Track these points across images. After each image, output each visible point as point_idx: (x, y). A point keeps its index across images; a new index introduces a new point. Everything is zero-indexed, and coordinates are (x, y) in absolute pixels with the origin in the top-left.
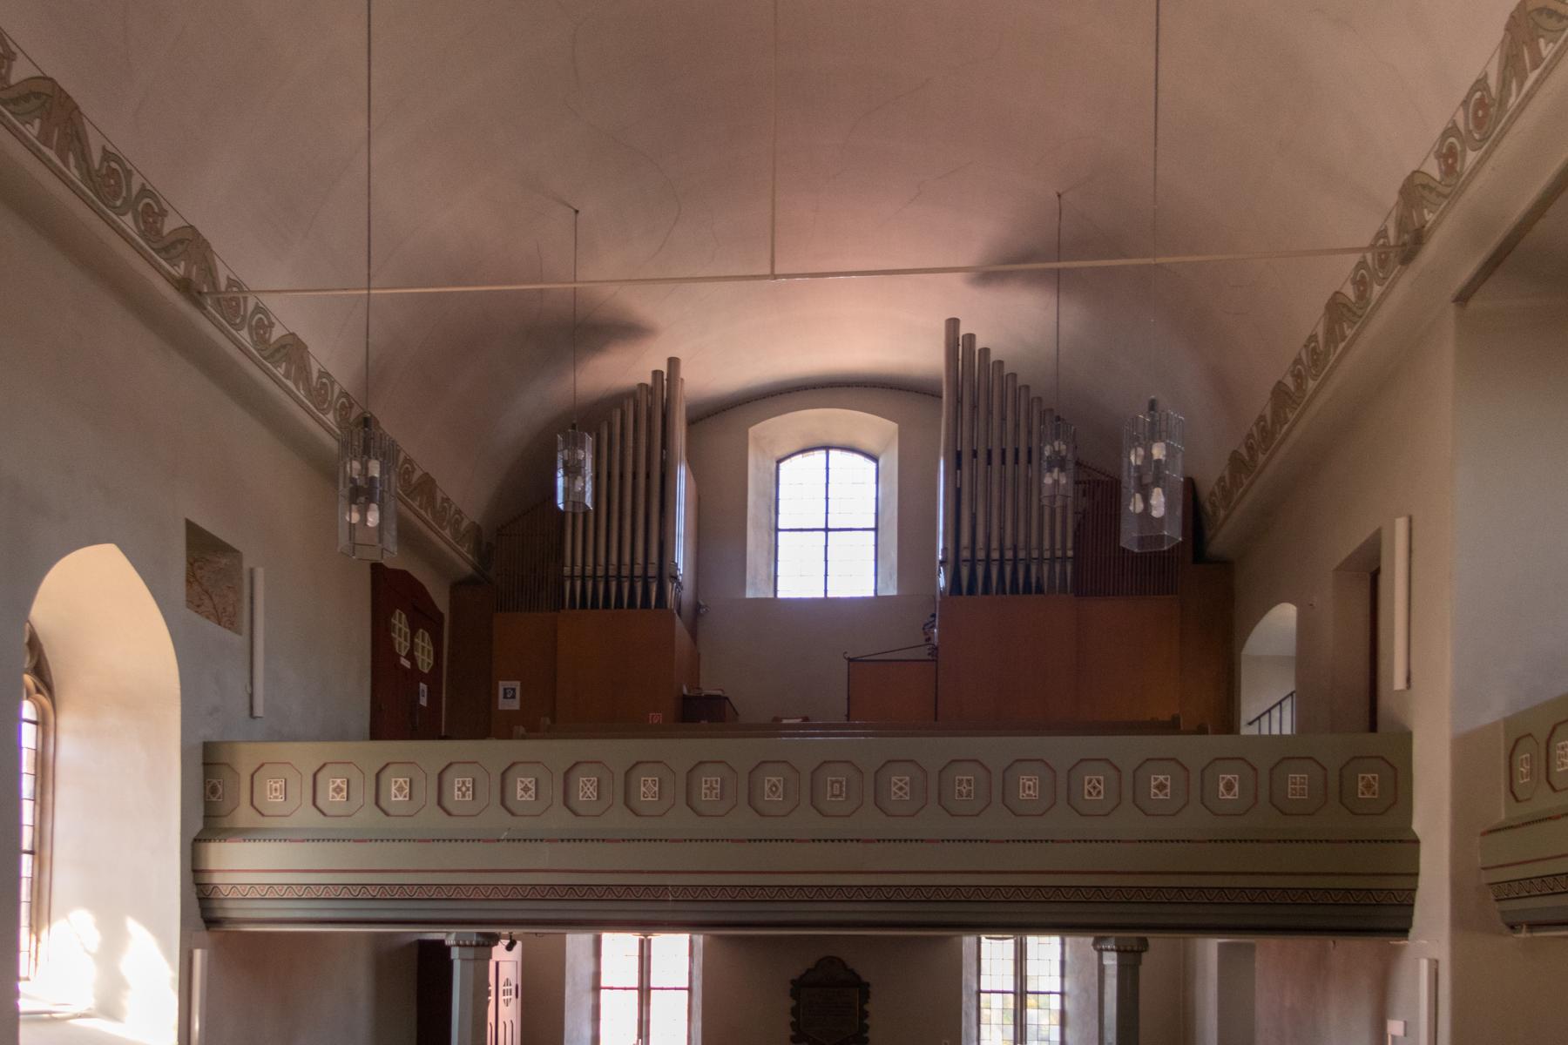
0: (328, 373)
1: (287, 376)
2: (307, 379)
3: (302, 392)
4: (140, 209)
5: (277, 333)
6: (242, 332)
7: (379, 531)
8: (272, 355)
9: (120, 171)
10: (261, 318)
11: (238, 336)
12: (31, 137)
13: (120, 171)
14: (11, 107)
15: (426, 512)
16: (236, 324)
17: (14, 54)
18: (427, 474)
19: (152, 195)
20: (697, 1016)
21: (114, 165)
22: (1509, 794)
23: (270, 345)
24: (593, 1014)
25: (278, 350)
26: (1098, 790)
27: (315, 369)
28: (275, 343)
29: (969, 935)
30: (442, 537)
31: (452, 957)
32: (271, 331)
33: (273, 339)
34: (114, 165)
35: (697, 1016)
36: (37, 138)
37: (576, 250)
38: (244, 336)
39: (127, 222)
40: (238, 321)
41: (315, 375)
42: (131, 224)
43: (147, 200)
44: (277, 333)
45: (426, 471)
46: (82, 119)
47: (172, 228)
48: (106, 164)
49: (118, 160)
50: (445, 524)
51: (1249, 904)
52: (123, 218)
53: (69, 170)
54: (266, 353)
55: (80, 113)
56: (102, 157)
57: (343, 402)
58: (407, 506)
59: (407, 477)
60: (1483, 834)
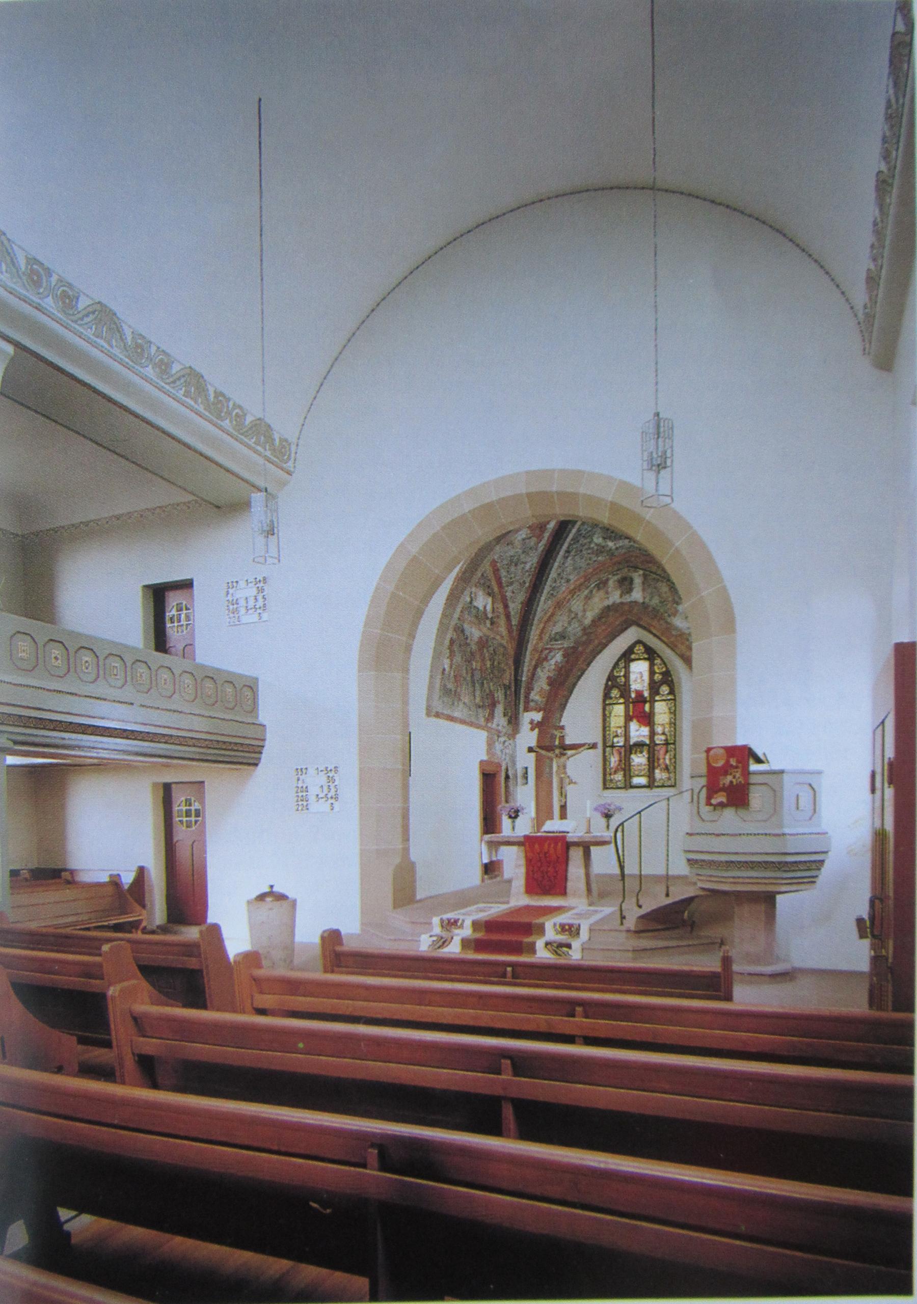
0: (141, 335)
7: (18, 347)
10: (64, 291)
15: (196, 402)
19: (240, 407)
22: (816, 789)
24: (686, 1043)
26: (130, 1063)
27: (276, 437)
30: (146, 379)
35: (816, 1192)
38: (226, 424)
39: (150, 371)
42: (152, 371)
43: (65, 288)
44: (249, 419)
48: (29, 267)
50: (223, 414)
52: (45, 300)
57: (237, 413)
58: (217, 427)
59: (67, 301)
60: (798, 796)
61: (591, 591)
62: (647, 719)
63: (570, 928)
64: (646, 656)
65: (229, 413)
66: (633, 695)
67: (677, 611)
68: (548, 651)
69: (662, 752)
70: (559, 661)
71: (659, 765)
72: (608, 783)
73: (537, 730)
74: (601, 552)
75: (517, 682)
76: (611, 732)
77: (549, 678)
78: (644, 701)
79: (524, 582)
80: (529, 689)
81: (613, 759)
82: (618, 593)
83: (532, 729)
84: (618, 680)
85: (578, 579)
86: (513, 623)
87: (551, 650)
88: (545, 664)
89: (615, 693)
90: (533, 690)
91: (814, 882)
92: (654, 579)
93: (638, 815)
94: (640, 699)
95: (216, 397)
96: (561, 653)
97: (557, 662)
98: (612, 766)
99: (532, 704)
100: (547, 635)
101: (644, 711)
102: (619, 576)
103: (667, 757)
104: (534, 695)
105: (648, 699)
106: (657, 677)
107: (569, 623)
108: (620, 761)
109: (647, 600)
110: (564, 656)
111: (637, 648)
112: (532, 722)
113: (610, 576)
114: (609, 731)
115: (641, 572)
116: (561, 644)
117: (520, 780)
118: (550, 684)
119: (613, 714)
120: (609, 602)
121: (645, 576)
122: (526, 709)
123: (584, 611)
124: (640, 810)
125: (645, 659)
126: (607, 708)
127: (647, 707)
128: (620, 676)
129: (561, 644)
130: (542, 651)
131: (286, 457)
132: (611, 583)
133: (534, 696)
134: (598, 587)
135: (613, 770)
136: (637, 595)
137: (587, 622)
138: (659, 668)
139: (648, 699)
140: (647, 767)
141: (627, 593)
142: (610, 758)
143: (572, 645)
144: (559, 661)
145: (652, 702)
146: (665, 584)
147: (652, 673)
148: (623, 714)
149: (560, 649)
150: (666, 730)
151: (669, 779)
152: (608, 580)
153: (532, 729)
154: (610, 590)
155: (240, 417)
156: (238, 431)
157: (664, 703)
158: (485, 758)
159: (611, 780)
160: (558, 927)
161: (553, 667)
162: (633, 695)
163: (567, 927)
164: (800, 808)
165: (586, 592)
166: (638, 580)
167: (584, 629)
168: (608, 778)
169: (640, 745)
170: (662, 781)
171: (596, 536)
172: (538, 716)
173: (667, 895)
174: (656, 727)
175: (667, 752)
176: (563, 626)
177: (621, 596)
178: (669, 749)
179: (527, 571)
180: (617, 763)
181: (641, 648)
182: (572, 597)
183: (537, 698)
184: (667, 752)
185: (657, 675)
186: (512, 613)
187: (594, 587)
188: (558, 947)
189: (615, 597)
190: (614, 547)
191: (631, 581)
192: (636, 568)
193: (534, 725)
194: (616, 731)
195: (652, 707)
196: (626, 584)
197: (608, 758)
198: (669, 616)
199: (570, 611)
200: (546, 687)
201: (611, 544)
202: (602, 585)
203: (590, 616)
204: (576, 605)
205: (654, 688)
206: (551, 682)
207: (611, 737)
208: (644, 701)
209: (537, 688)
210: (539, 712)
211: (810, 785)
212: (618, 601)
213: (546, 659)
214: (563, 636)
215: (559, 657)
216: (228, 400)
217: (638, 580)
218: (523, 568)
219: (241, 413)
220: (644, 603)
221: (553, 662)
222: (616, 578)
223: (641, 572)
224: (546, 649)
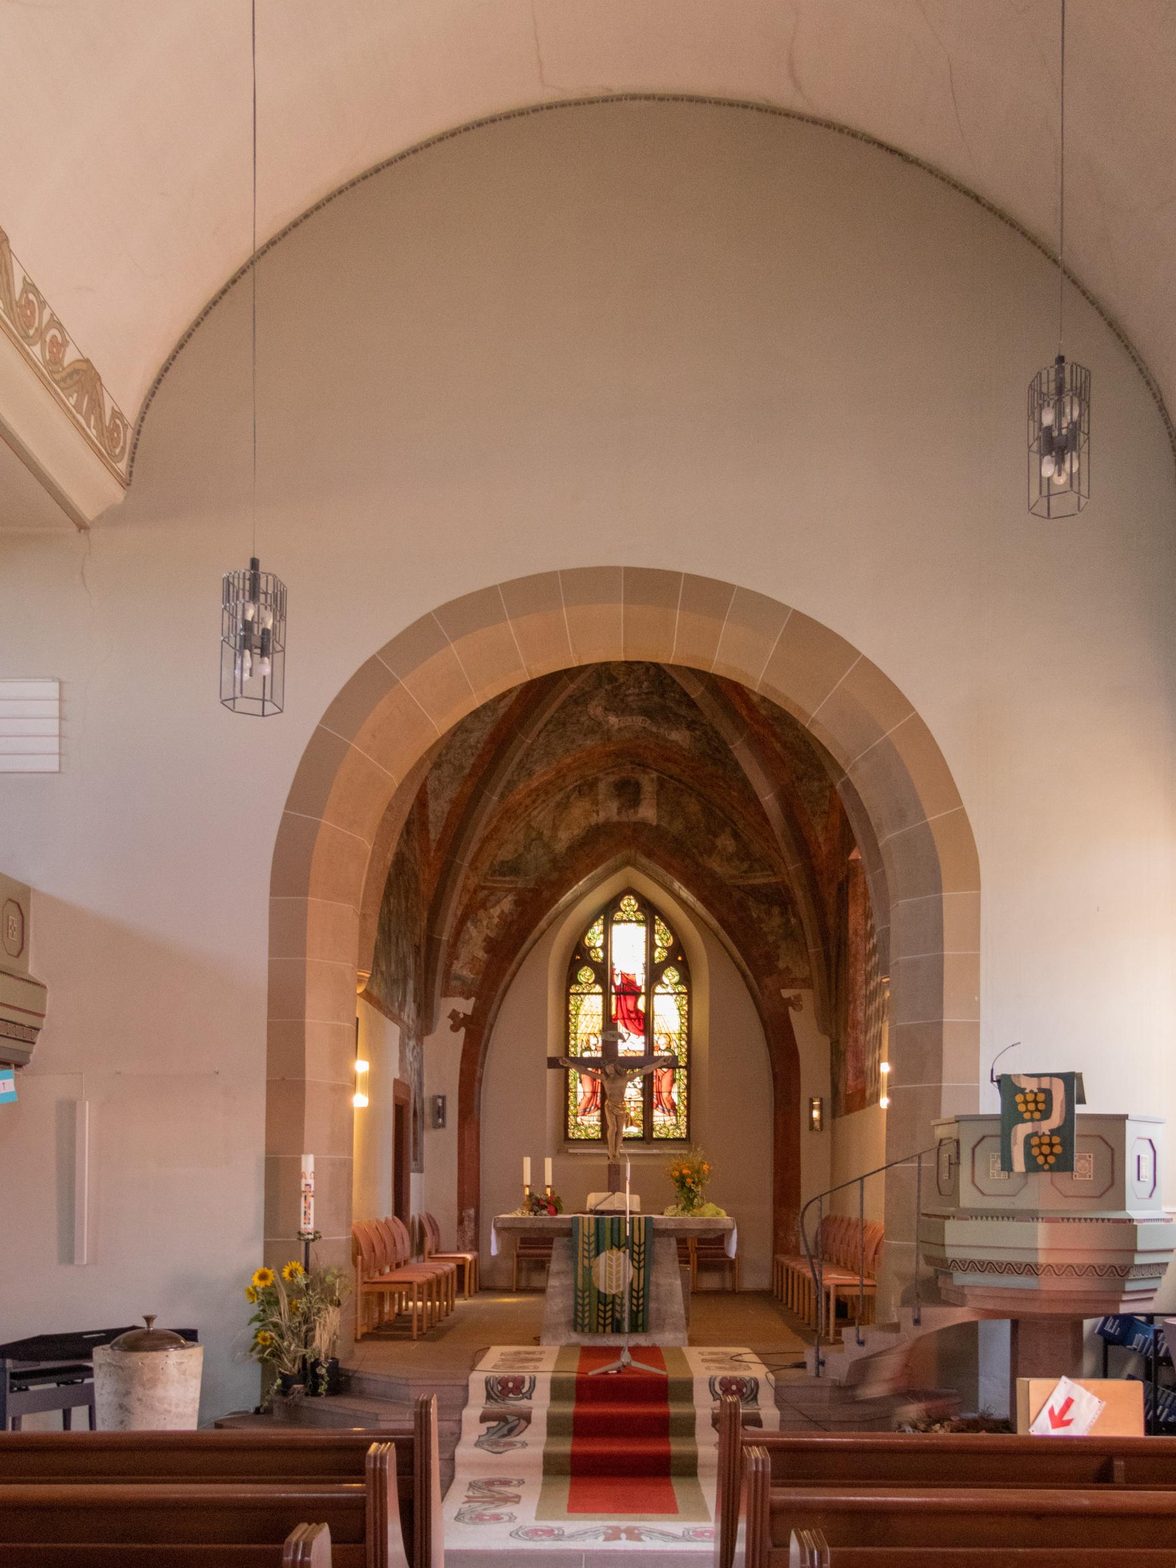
1: (77, 406)
2: (100, 418)
3: (94, 431)
4: (48, 339)
5: (70, 356)
6: (119, 465)
8: (64, 380)
9: (35, 301)
11: (30, 351)
12: (70, 406)
13: (35, 301)
14: (62, 384)
16: (115, 456)
17: (68, 342)
18: (87, 361)
19: (59, 326)
20: (704, 913)
21: (31, 297)
23: (64, 369)
25: (71, 375)
28: (69, 365)
29: (108, 1435)
31: (644, 976)
32: (65, 350)
33: (66, 363)
34: (31, 297)
36: (74, 407)
37: (254, 56)
38: (36, 351)
40: (118, 451)
41: (18, 287)
44: (70, 356)
45: (86, 355)
46: (752, 1349)
47: (69, 363)
49: (36, 292)
51: (663, 918)
53: (90, 429)
54: (57, 377)
55: (101, 384)
56: (23, 289)
57: (54, 337)
60: (1139, 1157)
61: (568, 797)
62: (644, 1023)
63: (739, 1390)
64: (641, 917)
65: (41, 333)
66: (618, 981)
67: (714, 847)
68: (486, 892)
69: (666, 1081)
70: (506, 911)
71: (660, 1102)
72: (570, 1132)
73: (463, 1030)
74: (593, 732)
75: (432, 942)
76: (579, 1042)
77: (488, 939)
78: (636, 993)
79: (462, 768)
80: (453, 956)
81: (580, 1088)
82: (614, 806)
83: (454, 1028)
84: (592, 955)
85: (545, 773)
86: (432, 836)
87: (493, 891)
88: (481, 913)
89: (586, 975)
90: (457, 958)
91: (1151, 1299)
92: (676, 789)
93: (859, 1181)
94: (629, 989)
95: (25, 291)
96: (510, 898)
97: (502, 911)
98: (579, 1099)
99: (454, 983)
100: (488, 864)
101: (637, 1011)
102: (617, 777)
103: (675, 1089)
104: (459, 968)
105: (643, 990)
106: (660, 955)
107: (527, 848)
108: (594, 1093)
109: (664, 824)
110: (516, 903)
111: (625, 902)
112: (454, 1015)
113: (601, 775)
114: (575, 1039)
115: (654, 775)
116: (512, 882)
117: (428, 1120)
118: (488, 950)
119: (582, 1012)
120: (601, 818)
121: (661, 784)
122: (446, 993)
123: (555, 828)
124: (862, 1175)
125: (638, 922)
126: (572, 999)
127: (641, 1004)
128: (594, 948)
129: (512, 882)
130: (475, 891)
131: (118, 451)
132: (602, 787)
133: (462, 969)
134: (579, 790)
135: (580, 1109)
136: (647, 812)
137: (561, 847)
138: (662, 939)
139: (643, 990)
140: (641, 1105)
141: (630, 807)
142: (576, 1087)
143: (532, 885)
144: (506, 911)
145: (650, 995)
146: (693, 800)
147: (651, 946)
148: (600, 1010)
149: (510, 890)
150: (674, 1045)
151: (677, 1126)
152: (596, 780)
153: (454, 1028)
154: (601, 797)
155: (59, 346)
156: (51, 372)
157: (671, 999)
158: (397, 1076)
159: (577, 1125)
160: (717, 1388)
161: (496, 920)
162: (618, 981)
163: (734, 1388)
164: (1141, 1179)
165: (558, 797)
166: (648, 786)
167: (554, 861)
168: (571, 1119)
169: (632, 1063)
170: (664, 1131)
171: (595, 703)
172: (465, 1006)
173: (917, 1322)
174: (656, 1037)
175: (673, 1081)
176: (516, 851)
177: (619, 813)
178: (677, 1076)
179: (471, 747)
180: (589, 1095)
181: (633, 902)
182: (534, 802)
183: (466, 973)
184: (673, 1081)
185: (659, 950)
186: (432, 817)
187: (573, 790)
188: (1059, 1420)
189: (610, 811)
190: (616, 727)
191: (638, 787)
192: (644, 766)
193: (457, 1021)
194: (588, 1041)
195: (649, 1004)
196: (629, 792)
197: (571, 1086)
198: (701, 854)
199: (529, 826)
200: (481, 954)
201: (613, 720)
202: (587, 788)
203: (565, 837)
204: (541, 817)
205: (654, 973)
206: (492, 946)
207: (579, 1050)
208: (636, 993)
209: (464, 953)
210: (467, 998)
211: (1150, 1141)
212: (615, 818)
213: (483, 905)
214: (512, 868)
215: (506, 904)
216: (43, 304)
217: (648, 786)
218: (464, 741)
219: (60, 340)
220: (658, 826)
221: (495, 912)
222: (611, 779)
223: (654, 775)
224: (483, 888)
